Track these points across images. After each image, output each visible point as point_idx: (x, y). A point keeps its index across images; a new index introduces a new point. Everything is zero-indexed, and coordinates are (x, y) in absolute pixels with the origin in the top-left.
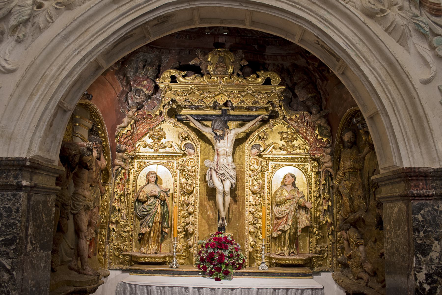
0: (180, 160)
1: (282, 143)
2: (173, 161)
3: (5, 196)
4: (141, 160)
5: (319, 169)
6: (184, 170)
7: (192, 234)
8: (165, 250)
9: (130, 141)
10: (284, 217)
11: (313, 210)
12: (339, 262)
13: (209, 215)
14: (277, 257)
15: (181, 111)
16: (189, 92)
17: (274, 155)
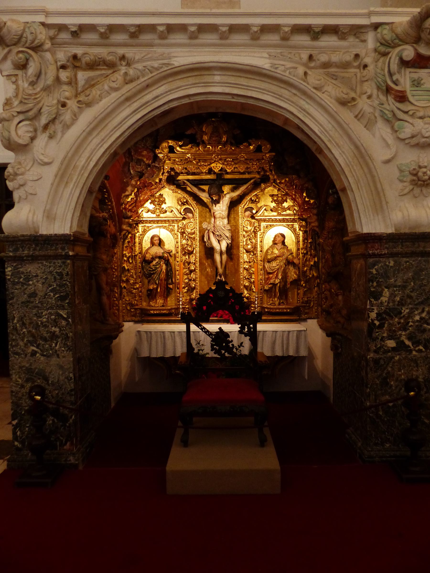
0: (180, 223)
1: (273, 205)
2: (173, 225)
3: (57, 264)
4: (144, 225)
5: (307, 228)
6: (184, 233)
7: (194, 288)
8: (171, 302)
9: (135, 208)
10: (275, 272)
11: (301, 265)
12: (323, 310)
13: (208, 272)
14: (268, 307)
15: (178, 177)
16: (186, 161)
17: (266, 216)
